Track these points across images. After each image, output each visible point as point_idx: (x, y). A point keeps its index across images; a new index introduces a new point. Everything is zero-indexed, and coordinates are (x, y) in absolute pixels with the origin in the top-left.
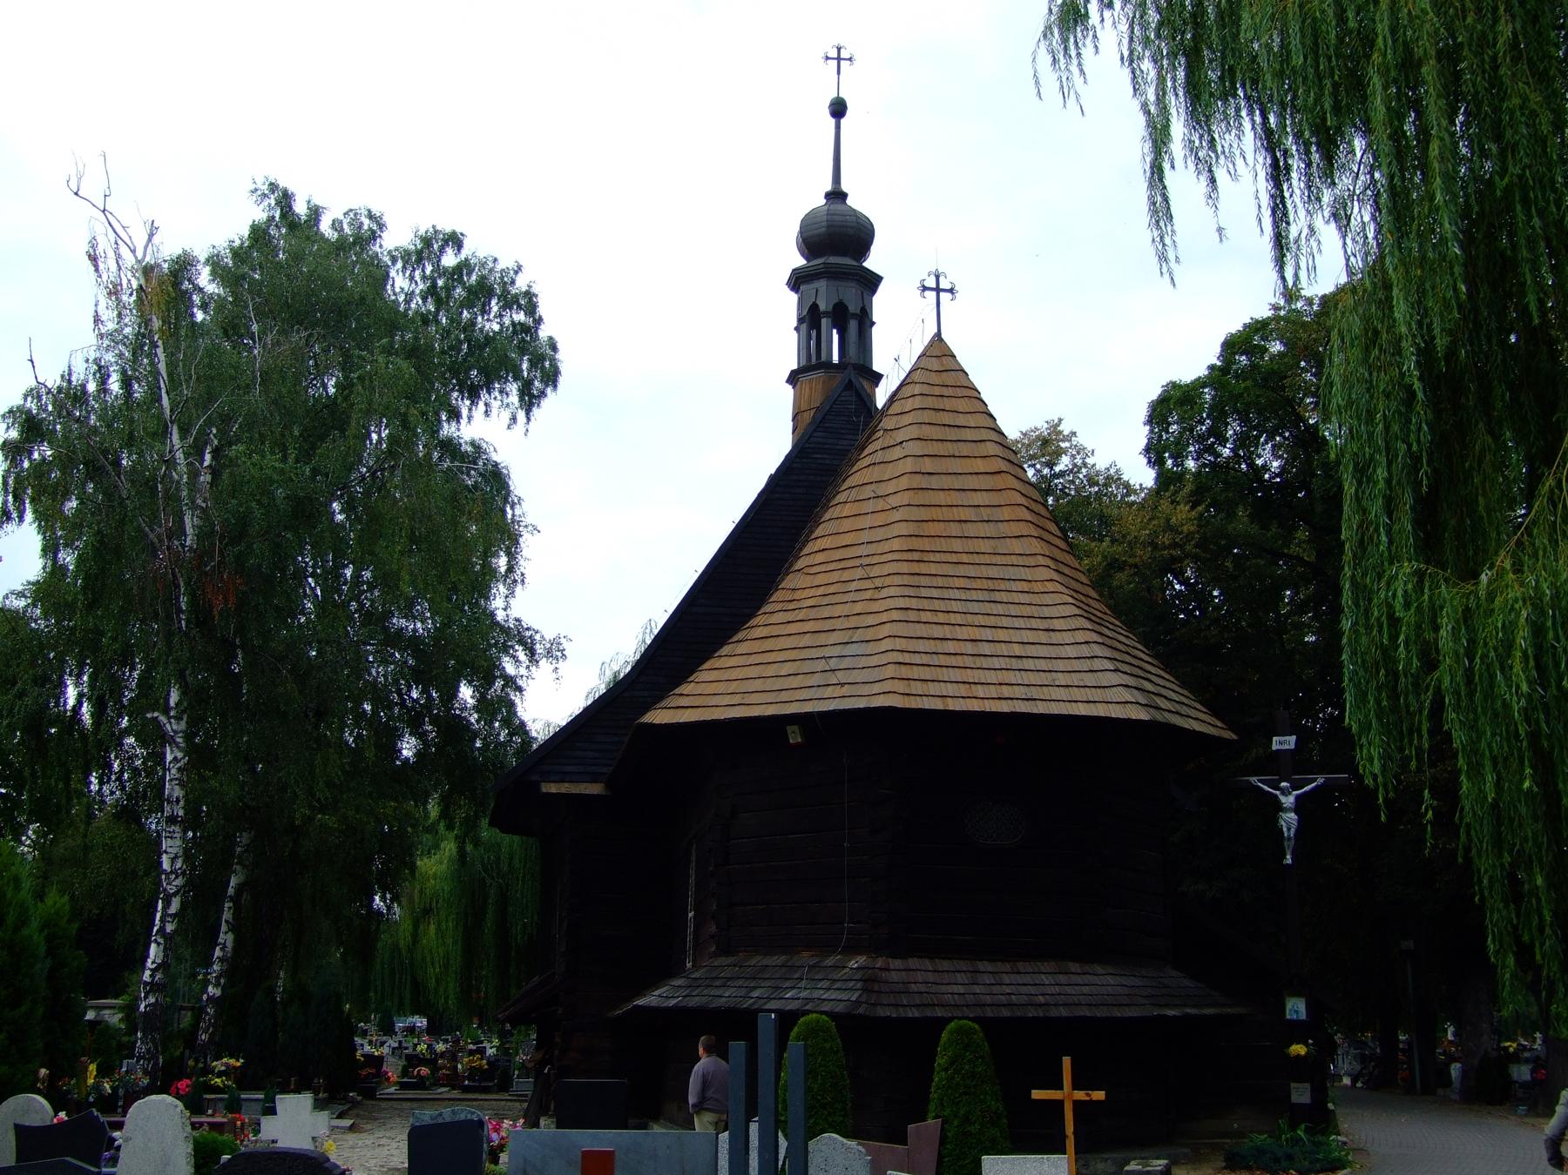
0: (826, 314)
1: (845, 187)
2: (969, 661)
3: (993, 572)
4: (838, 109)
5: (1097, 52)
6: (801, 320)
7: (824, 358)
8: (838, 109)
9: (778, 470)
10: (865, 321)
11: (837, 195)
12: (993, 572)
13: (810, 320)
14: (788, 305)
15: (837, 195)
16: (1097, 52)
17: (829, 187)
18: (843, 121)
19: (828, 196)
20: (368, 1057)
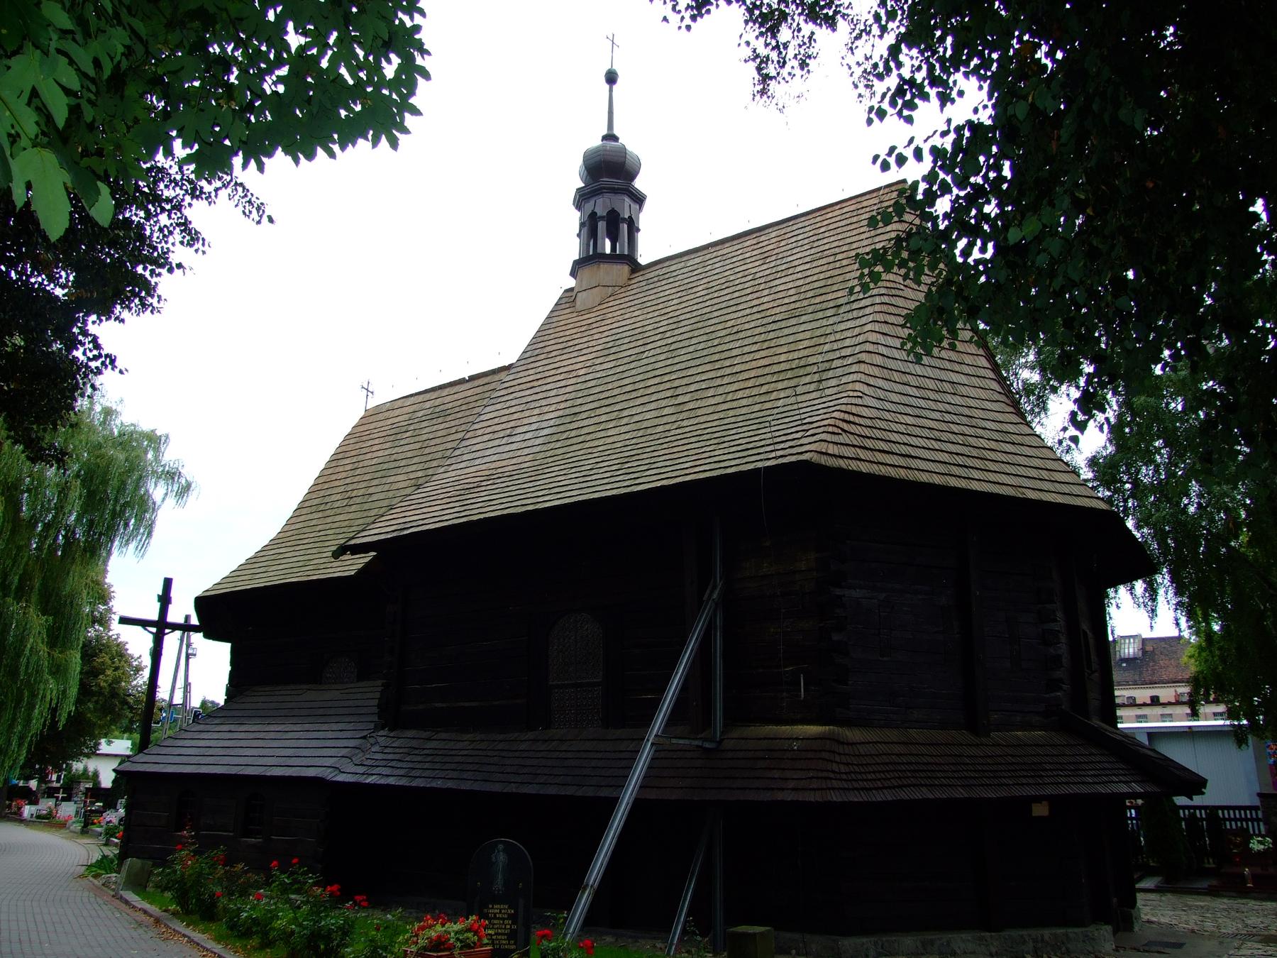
0: (602, 218)
1: (616, 132)
2: (535, 384)
3: (545, 388)
4: (611, 78)
5: (168, 583)
6: (582, 225)
7: (599, 251)
8: (611, 78)
9: (233, 663)
10: (633, 228)
11: (610, 137)
12: (545, 388)
13: (590, 228)
14: (573, 218)
15: (610, 137)
16: (168, 583)
17: (605, 132)
18: (615, 87)
19: (605, 138)
20: (75, 336)
